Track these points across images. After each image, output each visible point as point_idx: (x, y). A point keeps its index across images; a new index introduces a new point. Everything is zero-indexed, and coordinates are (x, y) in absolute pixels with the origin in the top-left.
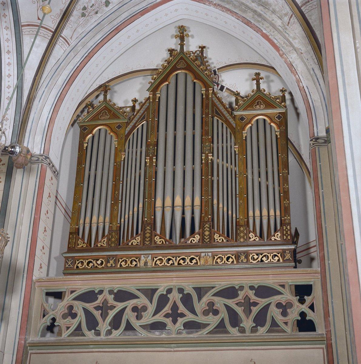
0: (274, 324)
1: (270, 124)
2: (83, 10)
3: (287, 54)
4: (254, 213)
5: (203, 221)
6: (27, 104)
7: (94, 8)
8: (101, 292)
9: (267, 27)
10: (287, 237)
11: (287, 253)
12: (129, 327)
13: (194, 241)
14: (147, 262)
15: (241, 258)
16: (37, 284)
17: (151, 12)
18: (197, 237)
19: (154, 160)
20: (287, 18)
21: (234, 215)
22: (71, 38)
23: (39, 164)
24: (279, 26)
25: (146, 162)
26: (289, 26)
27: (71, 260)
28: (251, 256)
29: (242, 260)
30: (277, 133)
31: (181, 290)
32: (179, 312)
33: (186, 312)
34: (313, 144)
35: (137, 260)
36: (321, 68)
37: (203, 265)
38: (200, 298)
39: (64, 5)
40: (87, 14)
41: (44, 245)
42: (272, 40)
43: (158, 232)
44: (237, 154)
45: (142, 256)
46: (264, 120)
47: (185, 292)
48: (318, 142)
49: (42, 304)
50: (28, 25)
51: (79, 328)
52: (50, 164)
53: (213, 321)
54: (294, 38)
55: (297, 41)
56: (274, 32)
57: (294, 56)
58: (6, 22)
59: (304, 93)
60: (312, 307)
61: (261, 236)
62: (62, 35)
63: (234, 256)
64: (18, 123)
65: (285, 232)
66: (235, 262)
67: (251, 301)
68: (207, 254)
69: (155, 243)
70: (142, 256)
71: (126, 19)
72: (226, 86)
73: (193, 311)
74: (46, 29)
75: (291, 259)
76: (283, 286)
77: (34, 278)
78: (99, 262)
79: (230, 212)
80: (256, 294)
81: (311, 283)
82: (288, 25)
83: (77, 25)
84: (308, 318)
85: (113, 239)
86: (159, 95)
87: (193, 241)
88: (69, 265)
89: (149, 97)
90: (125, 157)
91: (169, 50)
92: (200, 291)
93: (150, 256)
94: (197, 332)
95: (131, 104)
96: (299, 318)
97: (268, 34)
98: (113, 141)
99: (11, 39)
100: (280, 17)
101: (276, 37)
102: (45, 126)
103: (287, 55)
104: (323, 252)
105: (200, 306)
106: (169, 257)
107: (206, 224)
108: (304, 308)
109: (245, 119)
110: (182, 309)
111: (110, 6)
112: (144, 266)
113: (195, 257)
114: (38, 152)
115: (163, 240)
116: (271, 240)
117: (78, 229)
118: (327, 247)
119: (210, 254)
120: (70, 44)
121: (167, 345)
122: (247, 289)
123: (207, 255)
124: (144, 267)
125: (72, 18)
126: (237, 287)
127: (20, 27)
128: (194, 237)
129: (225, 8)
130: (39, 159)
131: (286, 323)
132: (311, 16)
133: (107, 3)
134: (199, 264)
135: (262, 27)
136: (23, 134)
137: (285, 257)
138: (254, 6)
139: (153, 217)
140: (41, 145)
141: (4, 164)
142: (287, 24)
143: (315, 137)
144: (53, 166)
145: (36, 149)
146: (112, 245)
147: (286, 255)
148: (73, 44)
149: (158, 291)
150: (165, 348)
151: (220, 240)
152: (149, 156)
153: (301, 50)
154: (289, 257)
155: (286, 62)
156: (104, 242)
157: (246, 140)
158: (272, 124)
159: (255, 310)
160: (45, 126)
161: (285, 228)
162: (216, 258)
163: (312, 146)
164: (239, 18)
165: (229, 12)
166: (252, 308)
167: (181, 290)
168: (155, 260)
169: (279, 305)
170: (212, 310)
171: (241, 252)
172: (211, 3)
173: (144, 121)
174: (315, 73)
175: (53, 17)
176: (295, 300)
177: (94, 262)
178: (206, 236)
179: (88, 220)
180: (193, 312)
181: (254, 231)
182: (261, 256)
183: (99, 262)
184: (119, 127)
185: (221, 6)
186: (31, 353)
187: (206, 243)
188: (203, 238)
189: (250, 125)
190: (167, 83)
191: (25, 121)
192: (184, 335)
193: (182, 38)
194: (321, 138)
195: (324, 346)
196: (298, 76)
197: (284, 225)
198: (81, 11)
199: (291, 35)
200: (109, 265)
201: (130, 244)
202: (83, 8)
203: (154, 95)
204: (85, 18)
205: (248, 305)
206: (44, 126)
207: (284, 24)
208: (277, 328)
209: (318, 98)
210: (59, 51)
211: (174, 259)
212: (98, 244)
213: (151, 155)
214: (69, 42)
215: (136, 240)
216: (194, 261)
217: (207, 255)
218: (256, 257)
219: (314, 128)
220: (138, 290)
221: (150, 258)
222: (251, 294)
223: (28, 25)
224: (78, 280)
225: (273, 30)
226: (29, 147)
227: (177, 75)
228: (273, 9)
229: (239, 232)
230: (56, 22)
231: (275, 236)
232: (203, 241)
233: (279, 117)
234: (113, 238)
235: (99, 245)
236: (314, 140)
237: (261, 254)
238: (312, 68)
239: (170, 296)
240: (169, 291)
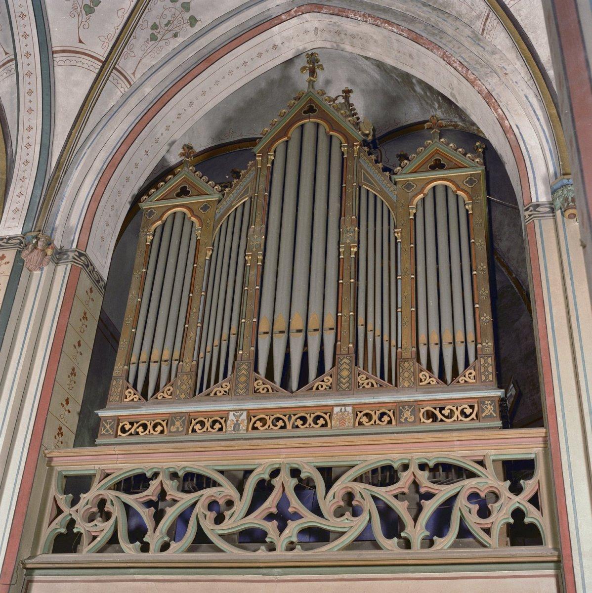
0: (464, 532)
3: (483, 79)
4: (429, 332)
6: (56, 171)
8: (156, 475)
10: (487, 377)
11: (487, 404)
12: (201, 539)
13: (322, 386)
14: (239, 425)
15: (403, 416)
18: (328, 380)
20: (480, 23)
22: (134, 74)
23: (67, 265)
24: (469, 36)
25: (246, 261)
26: (485, 35)
27: (110, 423)
29: (406, 418)
30: (467, 207)
31: (295, 473)
34: (530, 215)
35: (222, 421)
36: (539, 89)
37: (335, 427)
38: (328, 487)
39: (121, 20)
40: (159, 36)
41: (69, 397)
44: (399, 242)
45: (231, 413)
47: (303, 476)
48: (539, 211)
50: (63, 51)
51: (114, 540)
52: (87, 266)
53: (353, 526)
56: (459, 48)
57: (494, 81)
59: (512, 136)
63: (392, 411)
64: (38, 200)
65: (483, 370)
66: (394, 423)
68: (343, 408)
70: (231, 413)
74: (92, 57)
75: (495, 415)
76: (481, 463)
79: (386, 337)
81: (532, 456)
82: (482, 34)
84: (527, 520)
85: (184, 387)
86: (272, 158)
87: (320, 386)
92: (329, 475)
93: (245, 413)
96: (512, 521)
100: (469, 23)
101: (462, 55)
103: (482, 81)
104: (552, 398)
105: (329, 501)
107: (344, 358)
108: (521, 501)
112: (234, 430)
116: (458, 382)
118: (560, 388)
119: (349, 409)
120: (132, 83)
121: (265, 571)
123: (343, 410)
124: (234, 432)
127: (50, 53)
128: (323, 381)
131: (488, 531)
132: (519, 10)
135: (440, 42)
141: (8, 263)
142: (480, 32)
143: (533, 203)
146: (181, 396)
147: (485, 408)
149: (254, 473)
150: (263, 575)
151: (368, 384)
152: (252, 251)
153: (505, 69)
154: (491, 411)
156: (168, 392)
158: (459, 193)
159: (430, 507)
163: (529, 219)
164: (403, 32)
165: (387, 24)
167: (295, 473)
168: (253, 420)
169: (473, 497)
173: (245, 198)
174: (530, 103)
176: (504, 487)
178: (343, 378)
180: (316, 510)
184: (205, 208)
187: (344, 390)
188: (339, 382)
190: (286, 139)
192: (297, 552)
194: (543, 204)
196: (502, 110)
197: (482, 357)
202: (152, 26)
204: (156, 44)
207: (475, 34)
209: (536, 143)
210: (114, 92)
211: (286, 419)
212: (159, 395)
213: (254, 249)
214: (130, 80)
215: (222, 387)
217: (343, 410)
219: (531, 189)
220: (222, 472)
221: (244, 416)
222: (423, 477)
223: (63, 51)
224: (117, 453)
227: (302, 126)
228: (457, 12)
229: (401, 370)
230: (107, 46)
231: (465, 376)
232: (338, 387)
234: (184, 385)
236: (531, 208)
238: (525, 95)
239: (277, 482)
240: (275, 473)
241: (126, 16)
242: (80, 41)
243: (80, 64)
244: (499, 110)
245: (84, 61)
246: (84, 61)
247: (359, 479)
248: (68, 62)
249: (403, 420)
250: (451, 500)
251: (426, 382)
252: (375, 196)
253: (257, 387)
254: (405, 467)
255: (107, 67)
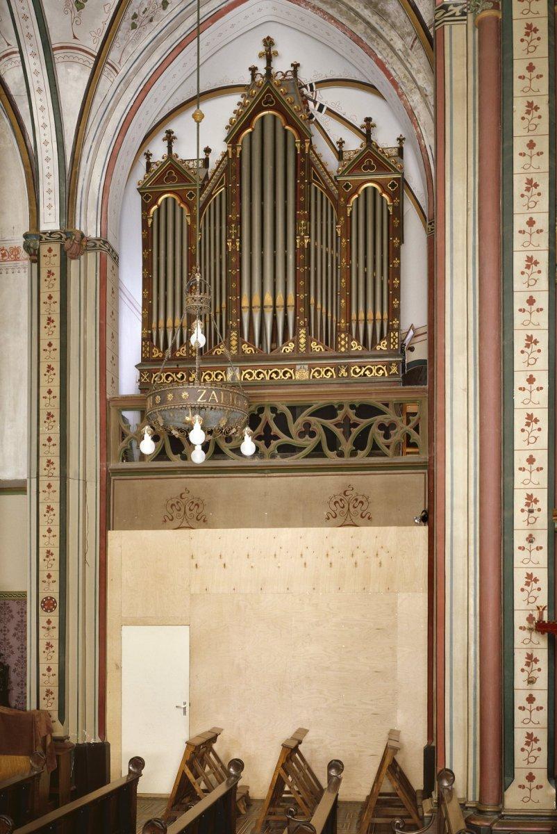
0: (375, 447)
1: (381, 195)
2: (133, 19)
4: (358, 314)
5: (298, 325)
6: (72, 167)
7: (147, 13)
9: (383, 49)
10: (394, 346)
16: (111, 404)
17: (226, 16)
19: (238, 244)
21: (334, 318)
26: (413, 50)
28: (353, 368)
31: (274, 409)
32: (272, 434)
33: (280, 434)
35: (223, 373)
38: (295, 419)
40: (138, 24)
42: (389, 71)
43: (246, 339)
46: (374, 189)
49: (120, 426)
50: (62, 48)
53: (309, 443)
54: (418, 72)
55: (421, 76)
58: (31, 45)
60: (416, 429)
61: (365, 344)
62: (109, 61)
65: (392, 340)
67: (351, 422)
69: (243, 352)
71: (189, 32)
72: (326, 106)
73: (287, 432)
74: (86, 52)
76: (387, 405)
77: (108, 397)
78: (179, 376)
79: (329, 315)
80: (357, 415)
83: (125, 42)
88: (145, 380)
89: (228, 151)
90: (201, 239)
91: (250, 69)
93: (238, 368)
94: (292, 456)
95: (202, 156)
97: (384, 61)
98: (185, 217)
99: (40, 71)
102: (98, 198)
105: (294, 428)
106: (260, 370)
109: (350, 186)
110: (275, 430)
111: (169, 8)
113: (289, 370)
114: (93, 236)
115: (252, 349)
117: (152, 334)
122: (347, 408)
125: (120, 34)
126: (336, 407)
128: (288, 345)
129: (327, 14)
130: (96, 244)
131: (388, 447)
133: (165, 4)
134: (293, 378)
136: (72, 211)
137: (390, 370)
138: (366, 13)
139: (238, 320)
140: (97, 225)
144: (113, 251)
145: (92, 232)
148: (122, 71)
155: (405, 105)
157: (351, 217)
158: (384, 195)
159: (355, 431)
160: (98, 198)
161: (392, 335)
162: (313, 371)
166: (352, 429)
169: (381, 427)
170: (308, 431)
171: (341, 365)
172: (308, 4)
175: (93, 34)
177: (174, 376)
179: (161, 324)
181: (357, 338)
182: (364, 369)
183: (179, 376)
185: (322, 11)
186: (114, 480)
189: (356, 196)
191: (73, 191)
193: (269, 60)
195: (426, 471)
198: (131, 21)
199: (415, 66)
200: (191, 379)
201: (214, 354)
203: (234, 148)
205: (347, 425)
206: (96, 198)
208: (378, 451)
210: (107, 84)
211: (265, 372)
216: (288, 375)
218: (358, 370)
222: (352, 413)
223: (62, 48)
225: (391, 54)
226: (83, 230)
228: (392, 22)
233: (393, 185)
235: (178, 355)
237: (364, 367)
241: (113, 11)
242: (75, 37)
243: (76, 60)
244: (419, 130)
245: (80, 56)
246: (80, 56)
247: (312, 415)
248: (66, 59)
249: (340, 375)
250: (368, 428)
251: (356, 348)
252: (322, 193)
253: (244, 349)
254: (341, 407)
255: (100, 61)
